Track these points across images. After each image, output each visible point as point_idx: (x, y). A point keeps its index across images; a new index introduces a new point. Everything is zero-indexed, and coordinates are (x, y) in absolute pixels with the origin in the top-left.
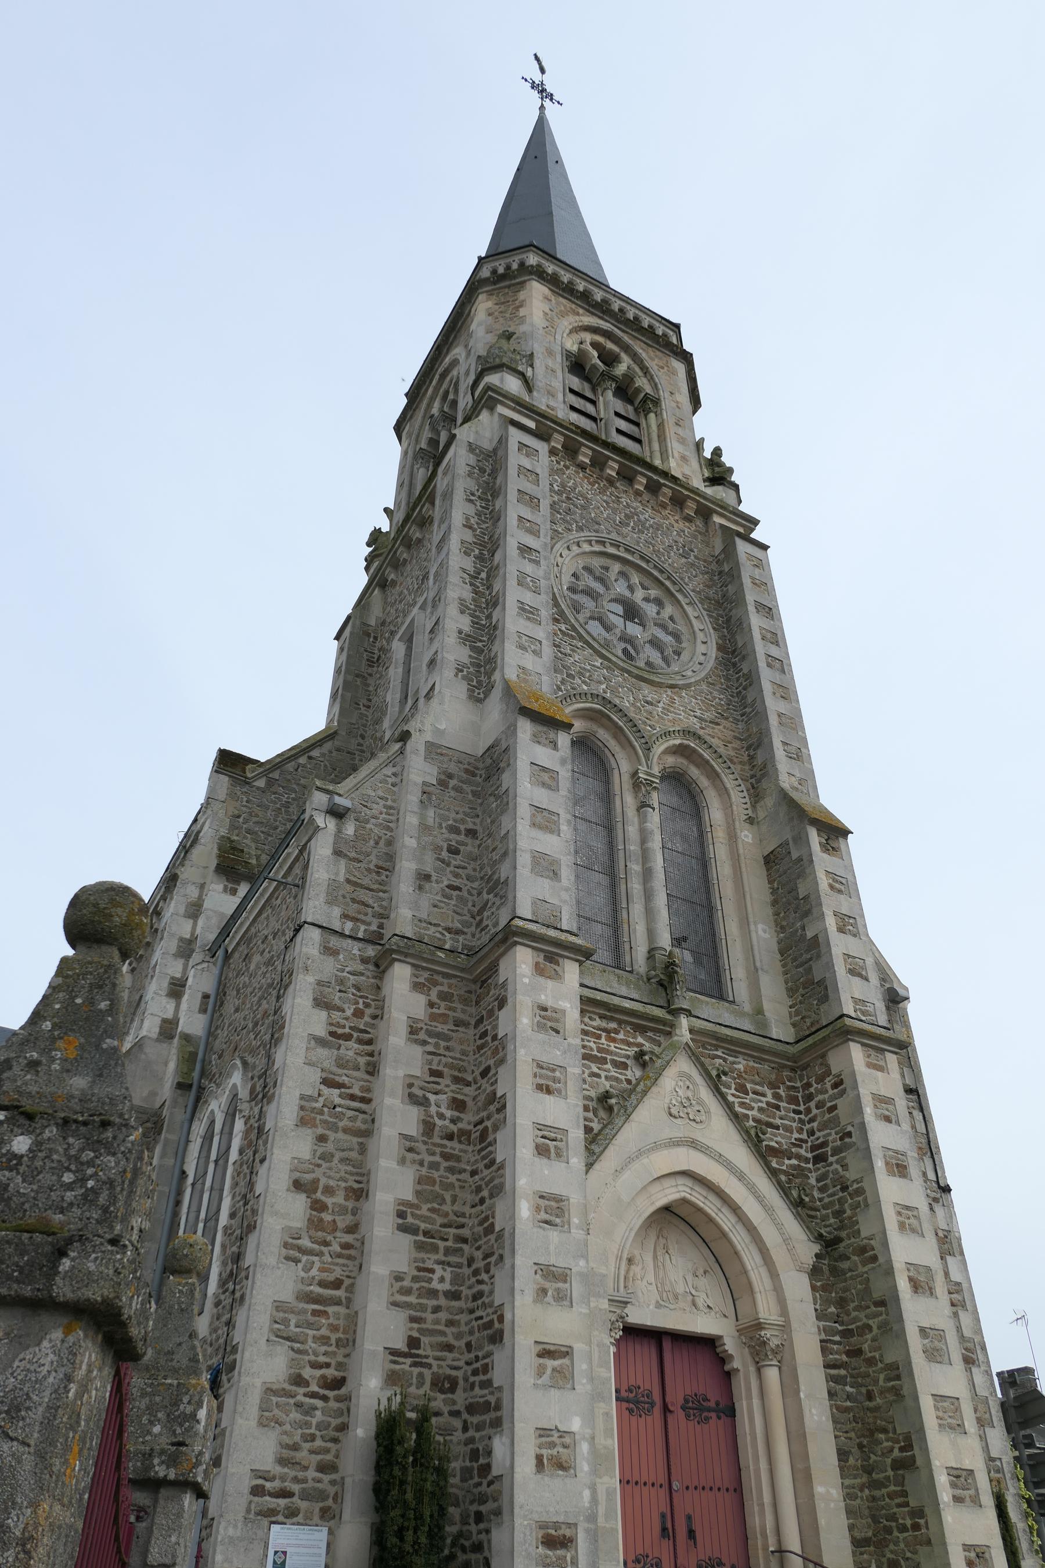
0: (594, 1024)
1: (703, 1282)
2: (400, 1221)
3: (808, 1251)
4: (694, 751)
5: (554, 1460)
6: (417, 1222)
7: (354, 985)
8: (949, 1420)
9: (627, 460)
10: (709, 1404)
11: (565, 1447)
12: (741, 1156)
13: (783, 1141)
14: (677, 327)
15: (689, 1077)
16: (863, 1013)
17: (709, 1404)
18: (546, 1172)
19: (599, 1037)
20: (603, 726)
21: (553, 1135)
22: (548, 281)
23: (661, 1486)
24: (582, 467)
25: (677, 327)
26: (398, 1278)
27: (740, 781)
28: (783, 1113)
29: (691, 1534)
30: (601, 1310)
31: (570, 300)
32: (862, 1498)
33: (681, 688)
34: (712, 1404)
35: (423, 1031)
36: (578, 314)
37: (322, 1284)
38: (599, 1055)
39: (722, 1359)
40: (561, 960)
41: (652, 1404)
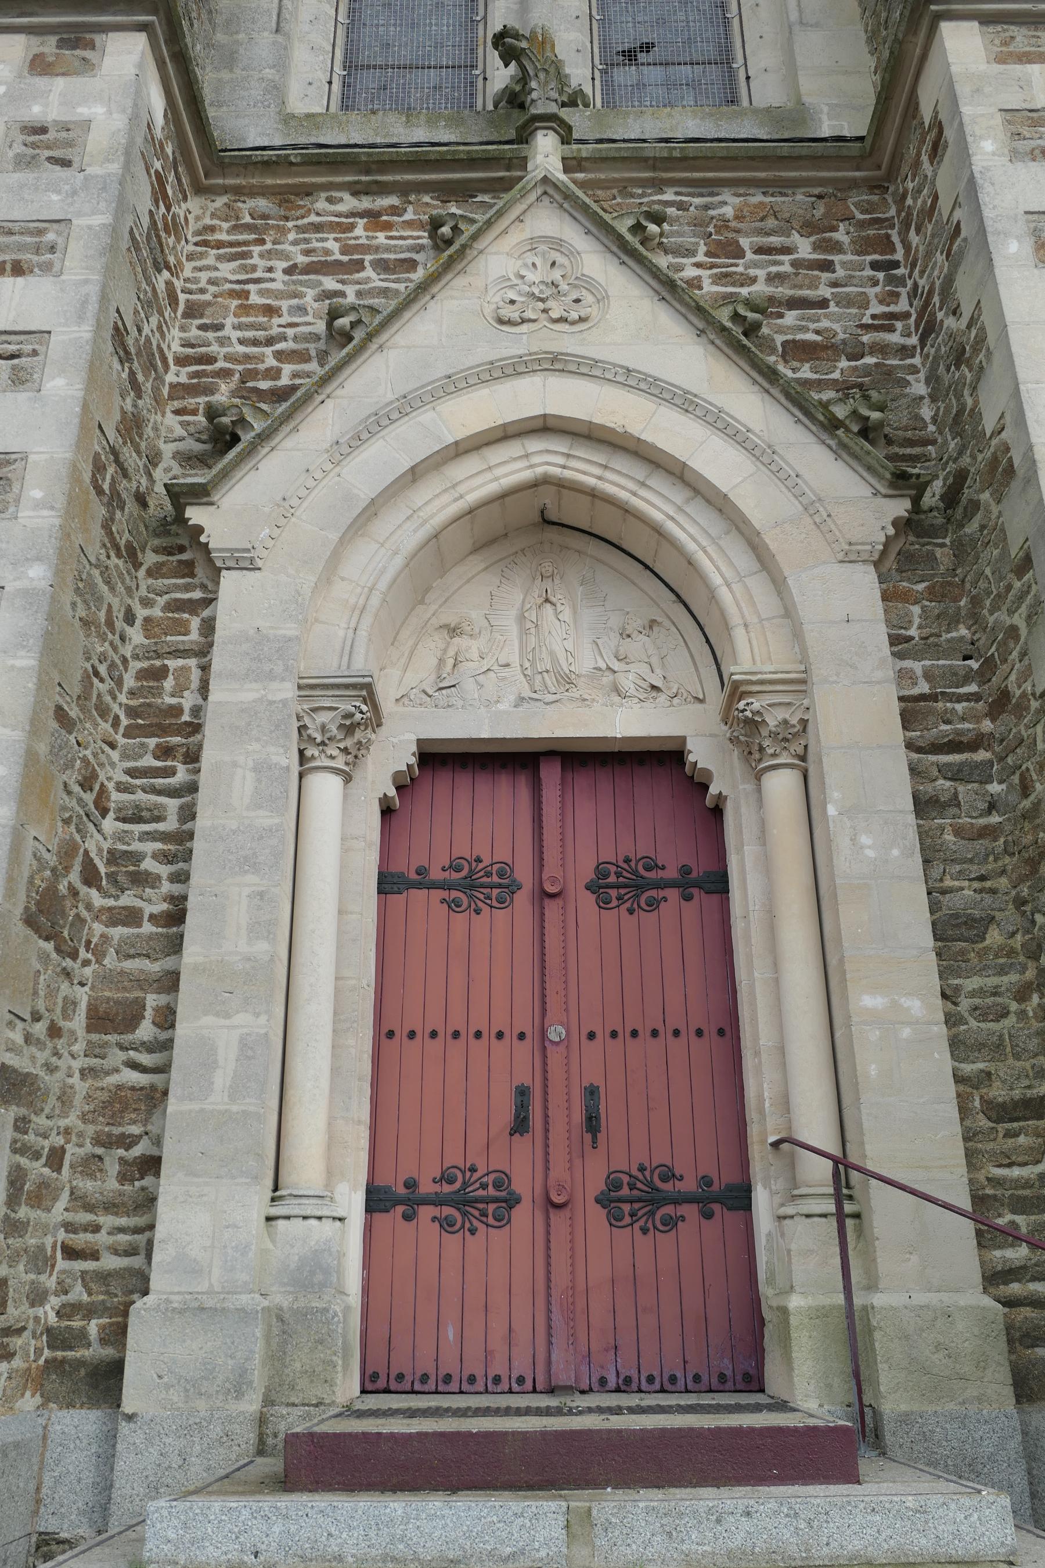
1: (639, 646)
3: (869, 512)
10: (661, 874)
12: (689, 360)
13: (836, 327)
15: (557, 244)
19: (352, 227)
21: (13, 348)
28: (841, 273)
29: (592, 1123)
30: (271, 703)
32: (1022, 1014)
34: (671, 873)
38: (345, 258)
39: (698, 785)
40: (98, 38)
41: (513, 888)
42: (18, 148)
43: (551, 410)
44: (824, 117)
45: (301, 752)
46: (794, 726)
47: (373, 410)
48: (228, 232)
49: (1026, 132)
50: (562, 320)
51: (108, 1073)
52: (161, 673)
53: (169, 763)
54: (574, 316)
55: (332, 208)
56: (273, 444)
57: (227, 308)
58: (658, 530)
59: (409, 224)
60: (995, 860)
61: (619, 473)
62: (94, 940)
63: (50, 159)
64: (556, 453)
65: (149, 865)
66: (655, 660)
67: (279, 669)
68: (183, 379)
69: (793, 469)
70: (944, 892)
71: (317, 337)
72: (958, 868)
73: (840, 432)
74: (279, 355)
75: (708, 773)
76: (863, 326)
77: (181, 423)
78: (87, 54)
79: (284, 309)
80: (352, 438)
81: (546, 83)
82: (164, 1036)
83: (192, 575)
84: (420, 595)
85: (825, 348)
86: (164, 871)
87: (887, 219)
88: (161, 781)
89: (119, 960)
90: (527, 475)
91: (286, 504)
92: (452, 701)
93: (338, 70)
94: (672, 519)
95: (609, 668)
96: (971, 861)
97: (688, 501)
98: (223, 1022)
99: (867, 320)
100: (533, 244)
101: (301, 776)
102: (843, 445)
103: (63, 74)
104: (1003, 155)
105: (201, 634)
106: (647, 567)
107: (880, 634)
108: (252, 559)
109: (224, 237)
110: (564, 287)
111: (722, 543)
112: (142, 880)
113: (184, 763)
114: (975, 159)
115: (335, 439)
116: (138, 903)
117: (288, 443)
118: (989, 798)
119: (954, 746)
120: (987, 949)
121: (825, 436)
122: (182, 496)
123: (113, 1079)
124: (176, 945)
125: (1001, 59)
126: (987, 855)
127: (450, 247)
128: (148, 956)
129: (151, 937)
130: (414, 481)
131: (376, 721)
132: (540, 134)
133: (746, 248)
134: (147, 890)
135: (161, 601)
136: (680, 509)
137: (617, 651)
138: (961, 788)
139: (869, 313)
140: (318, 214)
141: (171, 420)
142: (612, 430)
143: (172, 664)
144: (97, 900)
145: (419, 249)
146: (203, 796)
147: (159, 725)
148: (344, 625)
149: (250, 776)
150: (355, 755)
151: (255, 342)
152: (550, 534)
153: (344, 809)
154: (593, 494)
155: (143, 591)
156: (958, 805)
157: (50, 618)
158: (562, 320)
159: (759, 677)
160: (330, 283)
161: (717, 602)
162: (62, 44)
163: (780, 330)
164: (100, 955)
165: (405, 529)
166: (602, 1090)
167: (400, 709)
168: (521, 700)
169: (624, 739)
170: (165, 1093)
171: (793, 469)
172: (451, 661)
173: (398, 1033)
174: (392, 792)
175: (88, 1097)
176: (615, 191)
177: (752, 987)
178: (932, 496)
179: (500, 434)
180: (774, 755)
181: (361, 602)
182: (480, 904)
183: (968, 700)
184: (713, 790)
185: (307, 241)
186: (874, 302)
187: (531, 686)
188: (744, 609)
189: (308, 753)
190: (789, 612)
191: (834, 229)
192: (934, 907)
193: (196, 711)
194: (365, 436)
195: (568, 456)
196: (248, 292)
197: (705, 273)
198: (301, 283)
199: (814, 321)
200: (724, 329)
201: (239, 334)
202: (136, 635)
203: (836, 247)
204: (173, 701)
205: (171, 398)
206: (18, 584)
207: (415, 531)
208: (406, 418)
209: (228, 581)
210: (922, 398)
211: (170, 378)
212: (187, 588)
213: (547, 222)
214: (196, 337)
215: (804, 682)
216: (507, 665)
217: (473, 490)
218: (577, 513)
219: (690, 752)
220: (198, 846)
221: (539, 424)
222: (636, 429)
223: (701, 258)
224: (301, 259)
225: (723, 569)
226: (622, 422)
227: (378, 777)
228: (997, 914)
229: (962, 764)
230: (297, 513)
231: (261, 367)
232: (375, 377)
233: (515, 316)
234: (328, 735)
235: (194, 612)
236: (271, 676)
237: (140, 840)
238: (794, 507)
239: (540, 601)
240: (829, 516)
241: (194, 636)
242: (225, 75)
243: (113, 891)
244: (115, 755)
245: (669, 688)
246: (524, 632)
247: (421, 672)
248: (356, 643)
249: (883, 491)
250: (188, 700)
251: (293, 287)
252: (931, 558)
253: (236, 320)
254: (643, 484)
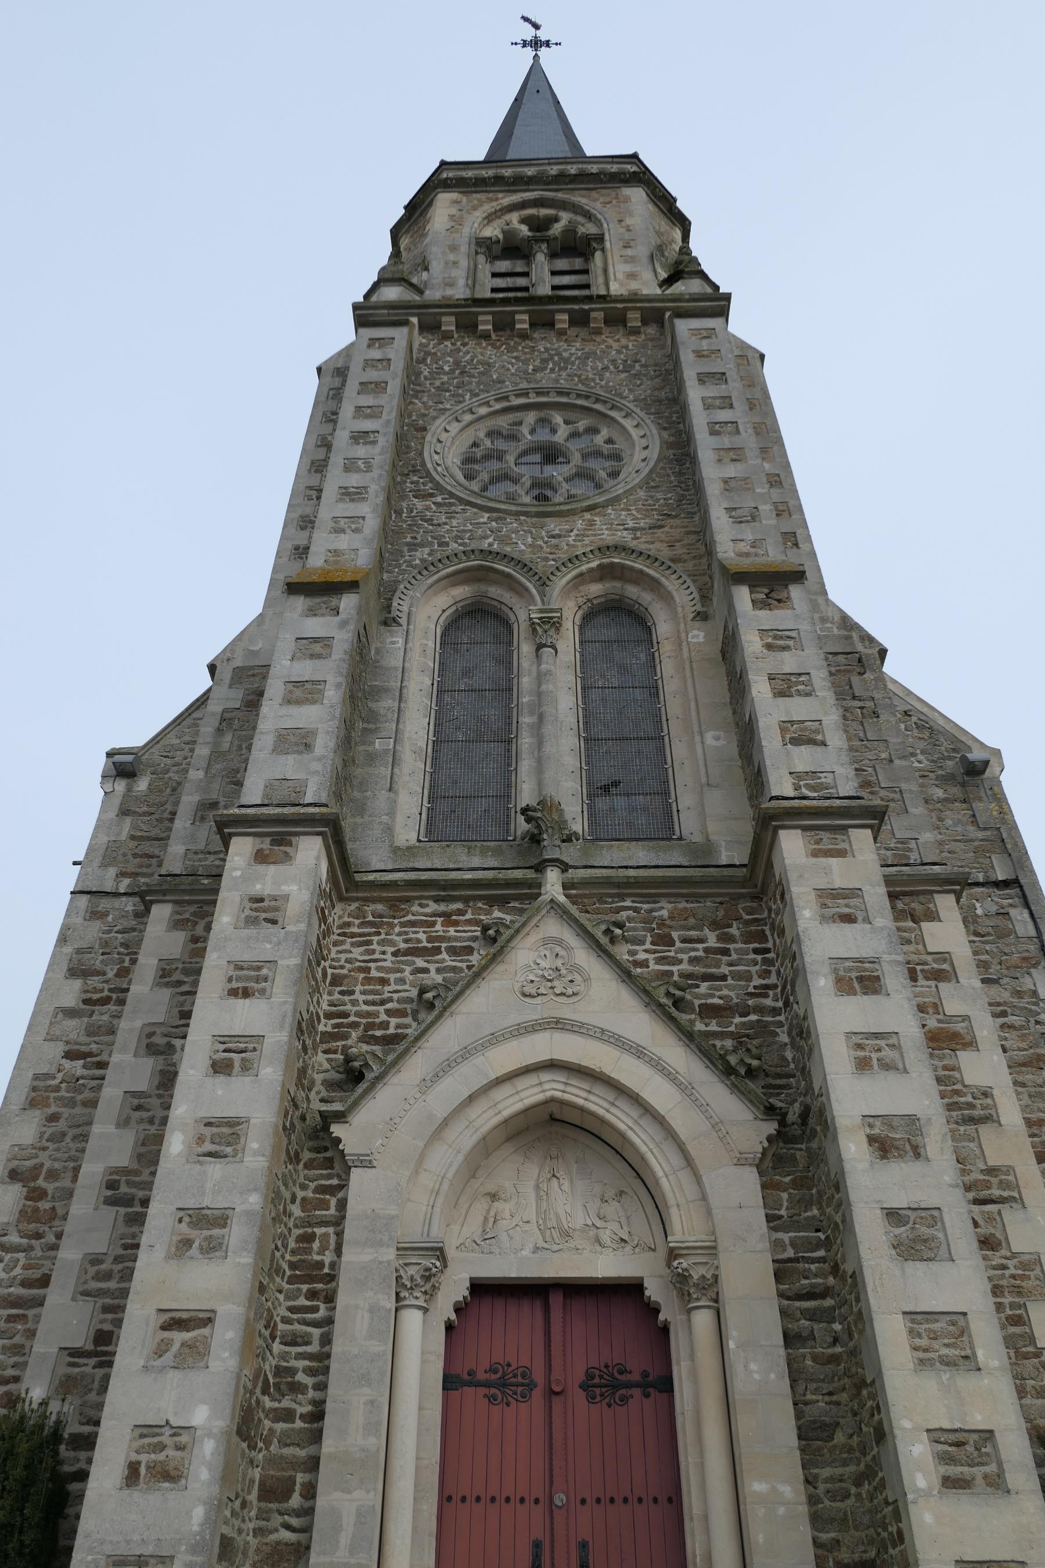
0: (427, 910)
1: (613, 1209)
2: (109, 1193)
3: (752, 1132)
4: (623, 566)
5: (158, 1468)
6: (134, 1191)
7: (122, 944)
8: (945, 1351)
9: (538, 305)
10: (629, 1377)
11: (180, 1448)
12: (639, 1023)
13: (732, 994)
14: (635, 156)
15: (560, 942)
16: (812, 788)
17: (629, 1377)
18: (220, 1093)
19: (433, 924)
20: (495, 583)
21: (242, 1045)
22: (455, 186)
23: (537, 1501)
24: (486, 336)
25: (635, 156)
26: (95, 1260)
27: (685, 577)
28: (734, 956)
30: (381, 1263)
31: (486, 191)
32: (859, 1495)
33: (604, 505)
34: (636, 1377)
35: (178, 972)
36: (497, 199)
37: (25, 1283)
38: (430, 945)
40: (294, 839)
41: (531, 1386)
42: (247, 912)
44: (723, 850)
45: (397, 1294)
48: (358, 927)
49: (829, 902)
50: (562, 994)
51: (271, 1532)
52: (309, 1238)
53: (315, 1303)
54: (570, 992)
55: (422, 910)
57: (357, 979)
59: (469, 922)
60: (839, 1380)
62: (265, 1433)
63: (265, 920)
65: (300, 1377)
67: (385, 1239)
68: (329, 1029)
70: (806, 1403)
71: (411, 1000)
72: (815, 1385)
73: (732, 1077)
74: (388, 1012)
76: (751, 995)
77: (327, 1059)
78: (287, 849)
79: (392, 980)
81: (553, 835)
82: (307, 1504)
83: (332, 1168)
85: (725, 1009)
86: (309, 1381)
87: (762, 919)
88: (309, 1316)
89: (280, 1448)
90: (541, 1097)
93: (425, 803)
94: (631, 1129)
96: (823, 1381)
97: (641, 1116)
98: (347, 1496)
99: (751, 990)
100: (546, 942)
101: (396, 1311)
103: (274, 863)
104: (816, 920)
105: (337, 1210)
107: (759, 1216)
108: (370, 1161)
109: (355, 930)
110: (564, 972)
111: (662, 1146)
112: (296, 1388)
113: (325, 1303)
114: (800, 923)
116: (294, 1406)
118: (833, 1334)
119: (810, 1296)
120: (835, 1447)
122: (328, 1119)
123: (273, 1537)
124: (317, 1437)
125: (815, 854)
126: (833, 1377)
127: (496, 942)
128: (298, 1445)
129: (301, 1430)
132: (549, 869)
133: (676, 939)
134: (299, 1396)
135: (312, 1185)
136: (636, 1122)
138: (816, 1327)
139: (752, 984)
140: (413, 915)
141: (321, 1057)
142: (594, 1070)
143: (319, 1231)
144: (268, 1403)
145: (474, 939)
146: (337, 1327)
147: (309, 1275)
148: (425, 1203)
149: (367, 1315)
150: (430, 1294)
151: (373, 1003)
152: (557, 1129)
153: (423, 1331)
155: (302, 1180)
156: (814, 1339)
157: (261, 1229)
158: (562, 994)
159: (686, 1244)
160: (420, 963)
162: (273, 843)
163: (698, 996)
164: (268, 1444)
165: (464, 1137)
166: (591, 1544)
168: (536, 1249)
169: (603, 1278)
170: (308, 1548)
172: (492, 1220)
173: (454, 1498)
174: (453, 1317)
175: (258, 1550)
176: (595, 900)
177: (687, 1467)
178: (793, 1116)
180: (698, 1299)
181: (437, 1187)
182: (510, 1399)
183: (819, 1262)
184: (661, 1317)
185: (406, 933)
186: (755, 977)
187: (544, 1237)
189: (402, 1295)
190: (704, 1198)
191: (730, 926)
192: (799, 1415)
193: (333, 1265)
194: (441, 1074)
195: (566, 1084)
196: (370, 968)
197: (651, 956)
198: (402, 962)
199: (718, 990)
200: (660, 1005)
201: (364, 997)
202: (296, 1210)
203: (731, 939)
204: (317, 1258)
205: (321, 1042)
206: (244, 1207)
209: (356, 1174)
210: (786, 1044)
211: (321, 1028)
212: (329, 1177)
213: (553, 927)
214: (338, 1000)
216: (528, 1222)
217: (506, 1108)
220: (334, 1366)
223: (648, 946)
224: (403, 946)
225: (664, 1165)
227: (444, 1308)
228: (841, 1420)
229: (816, 1309)
231: (377, 1020)
232: (449, 1034)
233: (534, 992)
235: (333, 1195)
236: (381, 1244)
237: (295, 1359)
239: (549, 1176)
241: (332, 1211)
242: (359, 820)
243: (277, 1396)
244: (281, 1297)
245: (633, 1241)
246: (539, 1198)
247: (473, 1228)
249: (760, 1117)
250: (328, 1258)
251: (397, 966)
252: (793, 1159)
253: (362, 988)
254: (613, 1104)
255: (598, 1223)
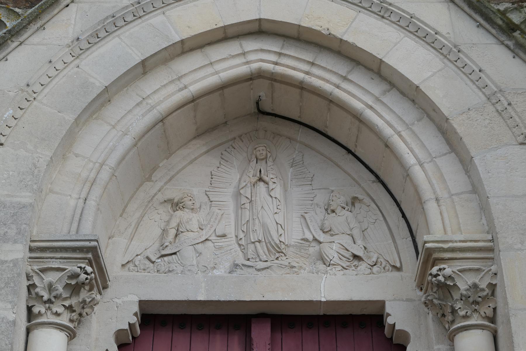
1: (341, 220)
43: (265, 15)
45: (29, 309)
46: (483, 290)
47: (110, 13)
56: (21, 39)
58: (358, 118)
61: (324, 69)
64: (269, 51)
66: (356, 233)
67: (12, 232)
69: (477, 65)
73: (517, 34)
75: (405, 335)
80: (91, 35)
84: (148, 173)
90: (244, 70)
91: (30, 90)
92: (173, 266)
94: (371, 108)
95: (315, 239)
97: (384, 93)
101: (28, 331)
102: (519, 45)
106: (349, 151)
111: (415, 128)
115: (76, 36)
117: (35, 39)
121: (503, 38)
130: (144, 73)
131: (101, 281)
136: (378, 99)
137: (323, 225)
142: (318, 33)
148: (75, 196)
150: (80, 315)
154: (302, 87)
159: (450, 245)
161: (411, 180)
167: (125, 273)
169: (329, 303)
171: (477, 65)
172: (173, 232)
179: (221, 35)
181: (92, 175)
187: (245, 254)
188: (436, 186)
189: (36, 310)
190: (476, 188)
194: (102, 34)
195: (280, 54)
207: (143, 115)
208: (140, 21)
215: (491, 250)
216: (224, 236)
218: (287, 103)
219: (388, 315)
221: (255, 27)
222: (338, 32)
225: (417, 151)
226: (326, 26)
230: (39, 98)
234: (54, 294)
238: (476, 98)
240: (509, 104)
246: (240, 207)
247: (147, 240)
248: (85, 212)
254: (345, 78)
255: (322, 237)
